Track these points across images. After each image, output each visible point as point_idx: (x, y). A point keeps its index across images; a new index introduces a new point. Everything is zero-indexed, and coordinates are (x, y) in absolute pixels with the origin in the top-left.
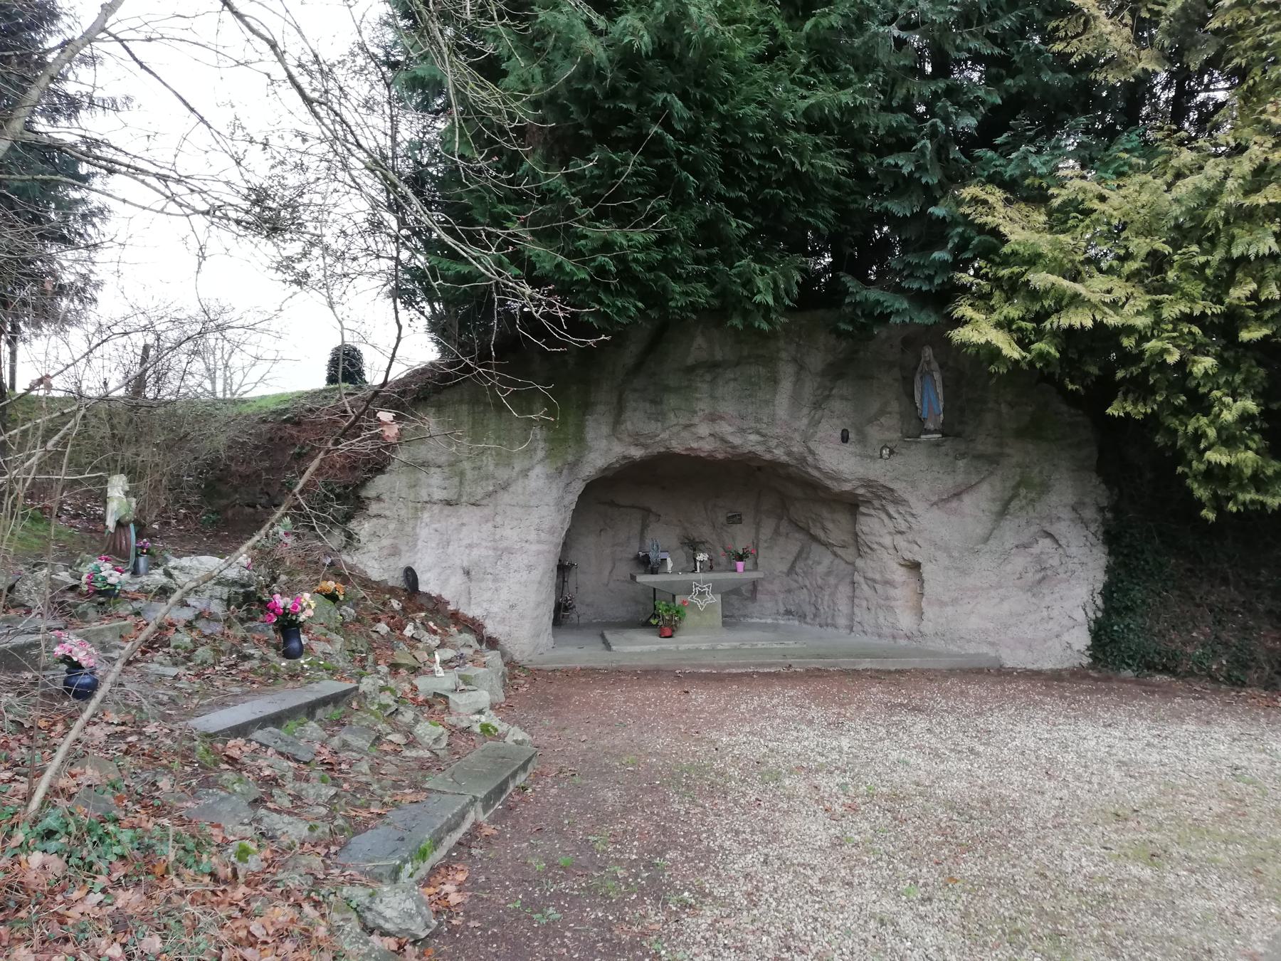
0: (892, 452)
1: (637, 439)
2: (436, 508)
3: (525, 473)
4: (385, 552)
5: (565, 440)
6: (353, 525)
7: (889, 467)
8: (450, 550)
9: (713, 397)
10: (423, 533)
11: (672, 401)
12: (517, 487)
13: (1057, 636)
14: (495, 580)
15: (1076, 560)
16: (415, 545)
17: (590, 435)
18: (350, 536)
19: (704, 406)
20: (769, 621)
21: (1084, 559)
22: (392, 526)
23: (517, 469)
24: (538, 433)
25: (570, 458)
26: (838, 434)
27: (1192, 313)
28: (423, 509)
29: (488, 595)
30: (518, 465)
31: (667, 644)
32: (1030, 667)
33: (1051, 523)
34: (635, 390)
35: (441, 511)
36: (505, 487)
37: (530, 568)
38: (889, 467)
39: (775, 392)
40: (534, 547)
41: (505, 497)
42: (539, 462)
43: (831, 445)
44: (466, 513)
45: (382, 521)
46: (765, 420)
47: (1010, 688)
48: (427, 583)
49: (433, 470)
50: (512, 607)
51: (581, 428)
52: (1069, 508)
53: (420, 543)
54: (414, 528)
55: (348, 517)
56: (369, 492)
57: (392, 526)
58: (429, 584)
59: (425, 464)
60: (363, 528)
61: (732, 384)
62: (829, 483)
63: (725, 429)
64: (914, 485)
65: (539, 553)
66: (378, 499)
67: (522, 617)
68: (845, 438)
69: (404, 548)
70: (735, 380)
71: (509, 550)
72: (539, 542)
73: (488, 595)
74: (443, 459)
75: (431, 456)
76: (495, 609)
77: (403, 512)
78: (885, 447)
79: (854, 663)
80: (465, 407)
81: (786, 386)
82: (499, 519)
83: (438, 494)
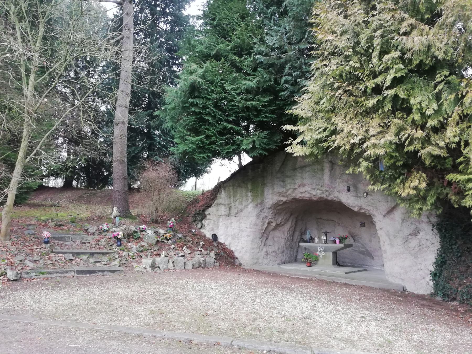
0: (367, 194)
1: (280, 194)
2: (224, 217)
3: (247, 206)
4: (210, 229)
5: (258, 196)
6: (203, 222)
7: (366, 201)
8: (228, 230)
9: (302, 178)
10: (221, 224)
11: (288, 180)
12: (245, 211)
13: (424, 278)
14: (238, 239)
15: (429, 242)
16: (218, 228)
17: (266, 193)
18: (203, 224)
19: (298, 181)
20: (379, 268)
21: (433, 242)
22: (212, 222)
23: (244, 205)
24: (250, 194)
25: (259, 201)
26: (346, 188)
27: (434, 110)
28: (220, 217)
29: (236, 244)
30: (244, 204)
31: (309, 269)
32: (416, 292)
33: (419, 223)
34: (277, 178)
35: (225, 218)
36: (242, 211)
37: (248, 236)
38: (366, 201)
39: (323, 174)
40: (249, 230)
41: (242, 214)
42: (250, 202)
43: (344, 193)
44: (233, 219)
45: (210, 220)
46: (320, 185)
47: (282, 282)
48: (221, 239)
49: (222, 206)
50: (243, 248)
51: (263, 192)
52: (426, 216)
53: (220, 227)
54: (218, 223)
55: (202, 219)
56: (207, 213)
57: (212, 222)
58: (221, 239)
59: (220, 204)
60: (205, 222)
61: (308, 173)
62: (351, 208)
63: (308, 189)
64: (376, 208)
65: (250, 232)
66: (209, 214)
67: (246, 252)
68: (349, 190)
69: (215, 228)
70: (309, 171)
71: (242, 231)
72: (251, 228)
73: (236, 244)
74: (226, 203)
75: (223, 202)
76: (238, 248)
77: (215, 218)
78: (365, 192)
79: (339, 280)
80: (231, 188)
81: (327, 172)
82: (241, 221)
83: (223, 213)
